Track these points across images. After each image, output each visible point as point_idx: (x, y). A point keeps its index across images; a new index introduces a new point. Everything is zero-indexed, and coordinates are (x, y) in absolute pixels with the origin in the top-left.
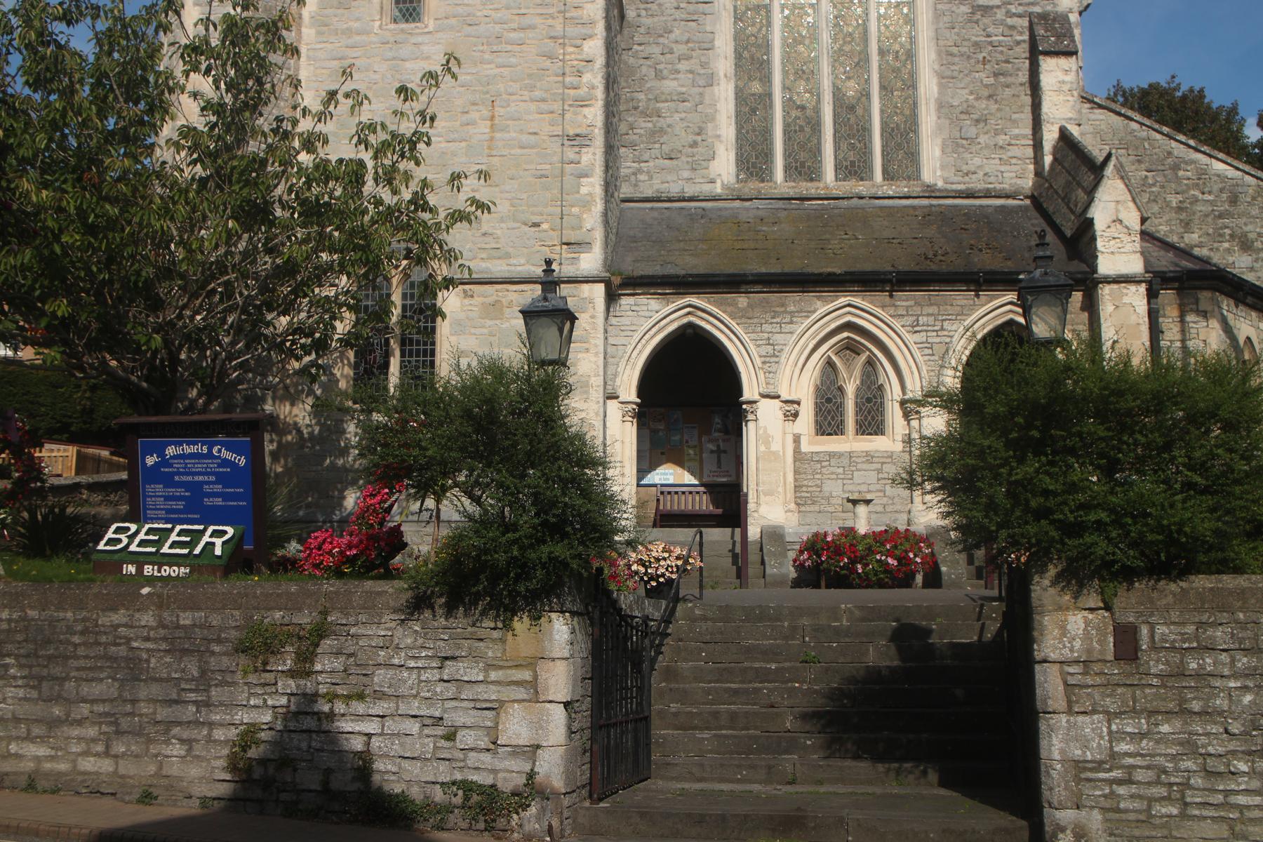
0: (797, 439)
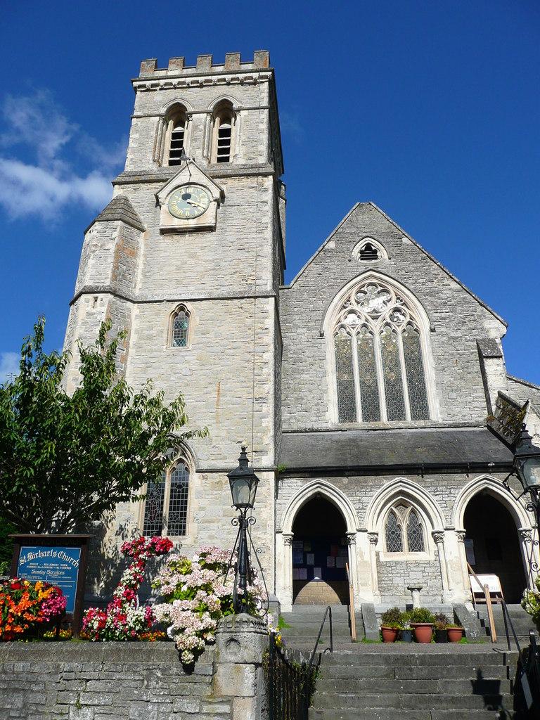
0: (378, 554)
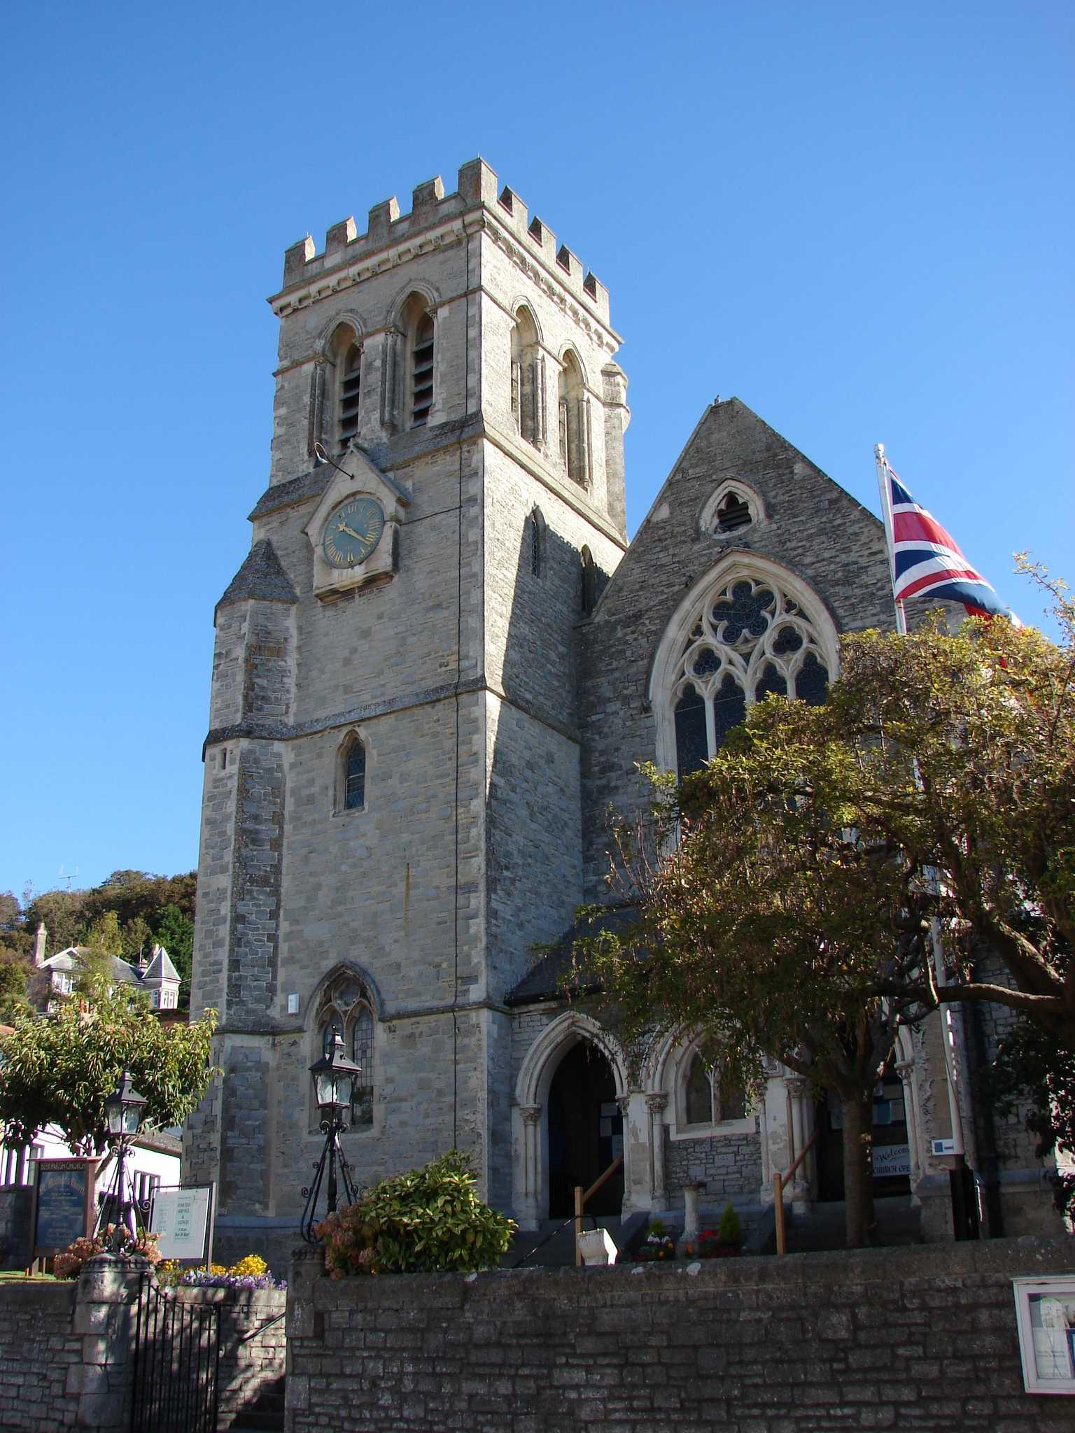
0: (665, 1129)
